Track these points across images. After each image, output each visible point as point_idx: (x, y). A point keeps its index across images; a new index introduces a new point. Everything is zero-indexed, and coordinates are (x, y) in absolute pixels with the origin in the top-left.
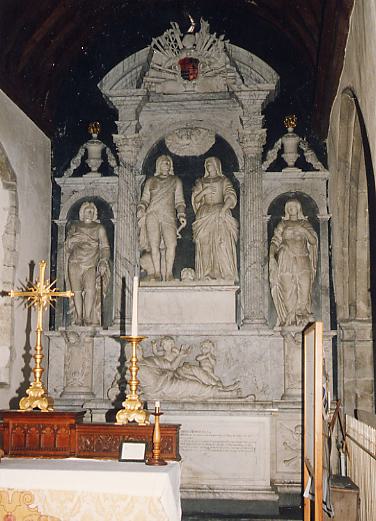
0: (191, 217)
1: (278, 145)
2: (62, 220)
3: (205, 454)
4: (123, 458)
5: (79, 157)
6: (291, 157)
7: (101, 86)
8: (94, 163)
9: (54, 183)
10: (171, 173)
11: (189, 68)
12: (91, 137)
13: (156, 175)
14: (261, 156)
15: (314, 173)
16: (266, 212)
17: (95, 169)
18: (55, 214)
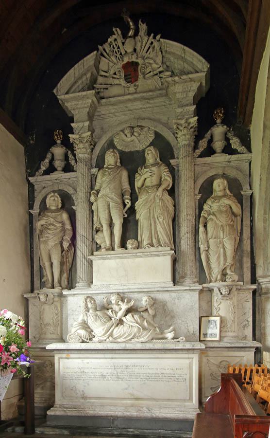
0: (134, 198)
1: (208, 135)
2: (35, 211)
3: (144, 383)
4: (219, 318)
5: (47, 161)
6: (218, 145)
7: (57, 91)
8: (58, 164)
9: (28, 181)
10: (118, 164)
11: (131, 71)
12: (56, 143)
13: (105, 166)
14: (193, 144)
15: (239, 155)
16: (197, 192)
17: (59, 169)
18: (31, 207)
